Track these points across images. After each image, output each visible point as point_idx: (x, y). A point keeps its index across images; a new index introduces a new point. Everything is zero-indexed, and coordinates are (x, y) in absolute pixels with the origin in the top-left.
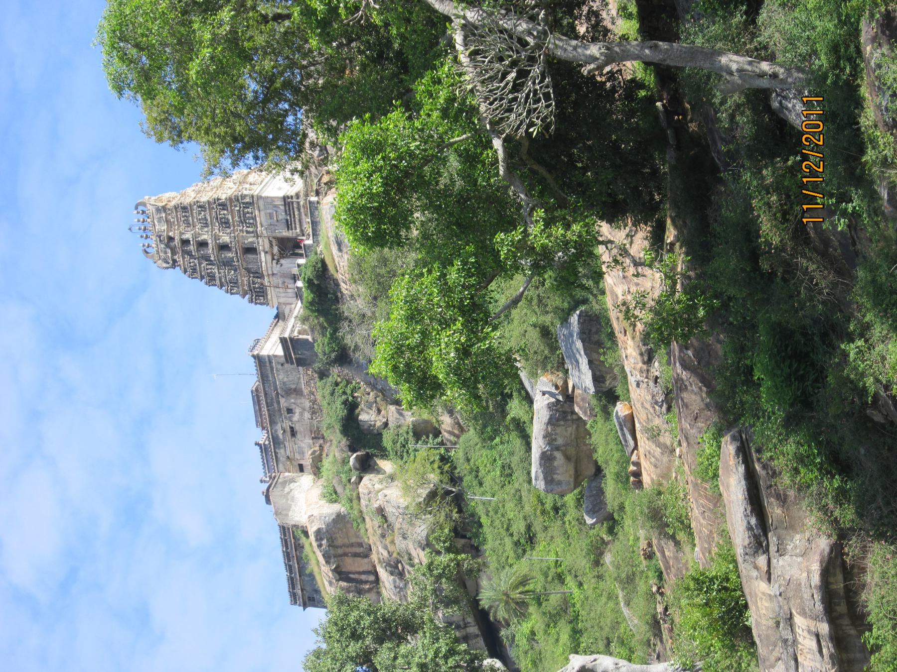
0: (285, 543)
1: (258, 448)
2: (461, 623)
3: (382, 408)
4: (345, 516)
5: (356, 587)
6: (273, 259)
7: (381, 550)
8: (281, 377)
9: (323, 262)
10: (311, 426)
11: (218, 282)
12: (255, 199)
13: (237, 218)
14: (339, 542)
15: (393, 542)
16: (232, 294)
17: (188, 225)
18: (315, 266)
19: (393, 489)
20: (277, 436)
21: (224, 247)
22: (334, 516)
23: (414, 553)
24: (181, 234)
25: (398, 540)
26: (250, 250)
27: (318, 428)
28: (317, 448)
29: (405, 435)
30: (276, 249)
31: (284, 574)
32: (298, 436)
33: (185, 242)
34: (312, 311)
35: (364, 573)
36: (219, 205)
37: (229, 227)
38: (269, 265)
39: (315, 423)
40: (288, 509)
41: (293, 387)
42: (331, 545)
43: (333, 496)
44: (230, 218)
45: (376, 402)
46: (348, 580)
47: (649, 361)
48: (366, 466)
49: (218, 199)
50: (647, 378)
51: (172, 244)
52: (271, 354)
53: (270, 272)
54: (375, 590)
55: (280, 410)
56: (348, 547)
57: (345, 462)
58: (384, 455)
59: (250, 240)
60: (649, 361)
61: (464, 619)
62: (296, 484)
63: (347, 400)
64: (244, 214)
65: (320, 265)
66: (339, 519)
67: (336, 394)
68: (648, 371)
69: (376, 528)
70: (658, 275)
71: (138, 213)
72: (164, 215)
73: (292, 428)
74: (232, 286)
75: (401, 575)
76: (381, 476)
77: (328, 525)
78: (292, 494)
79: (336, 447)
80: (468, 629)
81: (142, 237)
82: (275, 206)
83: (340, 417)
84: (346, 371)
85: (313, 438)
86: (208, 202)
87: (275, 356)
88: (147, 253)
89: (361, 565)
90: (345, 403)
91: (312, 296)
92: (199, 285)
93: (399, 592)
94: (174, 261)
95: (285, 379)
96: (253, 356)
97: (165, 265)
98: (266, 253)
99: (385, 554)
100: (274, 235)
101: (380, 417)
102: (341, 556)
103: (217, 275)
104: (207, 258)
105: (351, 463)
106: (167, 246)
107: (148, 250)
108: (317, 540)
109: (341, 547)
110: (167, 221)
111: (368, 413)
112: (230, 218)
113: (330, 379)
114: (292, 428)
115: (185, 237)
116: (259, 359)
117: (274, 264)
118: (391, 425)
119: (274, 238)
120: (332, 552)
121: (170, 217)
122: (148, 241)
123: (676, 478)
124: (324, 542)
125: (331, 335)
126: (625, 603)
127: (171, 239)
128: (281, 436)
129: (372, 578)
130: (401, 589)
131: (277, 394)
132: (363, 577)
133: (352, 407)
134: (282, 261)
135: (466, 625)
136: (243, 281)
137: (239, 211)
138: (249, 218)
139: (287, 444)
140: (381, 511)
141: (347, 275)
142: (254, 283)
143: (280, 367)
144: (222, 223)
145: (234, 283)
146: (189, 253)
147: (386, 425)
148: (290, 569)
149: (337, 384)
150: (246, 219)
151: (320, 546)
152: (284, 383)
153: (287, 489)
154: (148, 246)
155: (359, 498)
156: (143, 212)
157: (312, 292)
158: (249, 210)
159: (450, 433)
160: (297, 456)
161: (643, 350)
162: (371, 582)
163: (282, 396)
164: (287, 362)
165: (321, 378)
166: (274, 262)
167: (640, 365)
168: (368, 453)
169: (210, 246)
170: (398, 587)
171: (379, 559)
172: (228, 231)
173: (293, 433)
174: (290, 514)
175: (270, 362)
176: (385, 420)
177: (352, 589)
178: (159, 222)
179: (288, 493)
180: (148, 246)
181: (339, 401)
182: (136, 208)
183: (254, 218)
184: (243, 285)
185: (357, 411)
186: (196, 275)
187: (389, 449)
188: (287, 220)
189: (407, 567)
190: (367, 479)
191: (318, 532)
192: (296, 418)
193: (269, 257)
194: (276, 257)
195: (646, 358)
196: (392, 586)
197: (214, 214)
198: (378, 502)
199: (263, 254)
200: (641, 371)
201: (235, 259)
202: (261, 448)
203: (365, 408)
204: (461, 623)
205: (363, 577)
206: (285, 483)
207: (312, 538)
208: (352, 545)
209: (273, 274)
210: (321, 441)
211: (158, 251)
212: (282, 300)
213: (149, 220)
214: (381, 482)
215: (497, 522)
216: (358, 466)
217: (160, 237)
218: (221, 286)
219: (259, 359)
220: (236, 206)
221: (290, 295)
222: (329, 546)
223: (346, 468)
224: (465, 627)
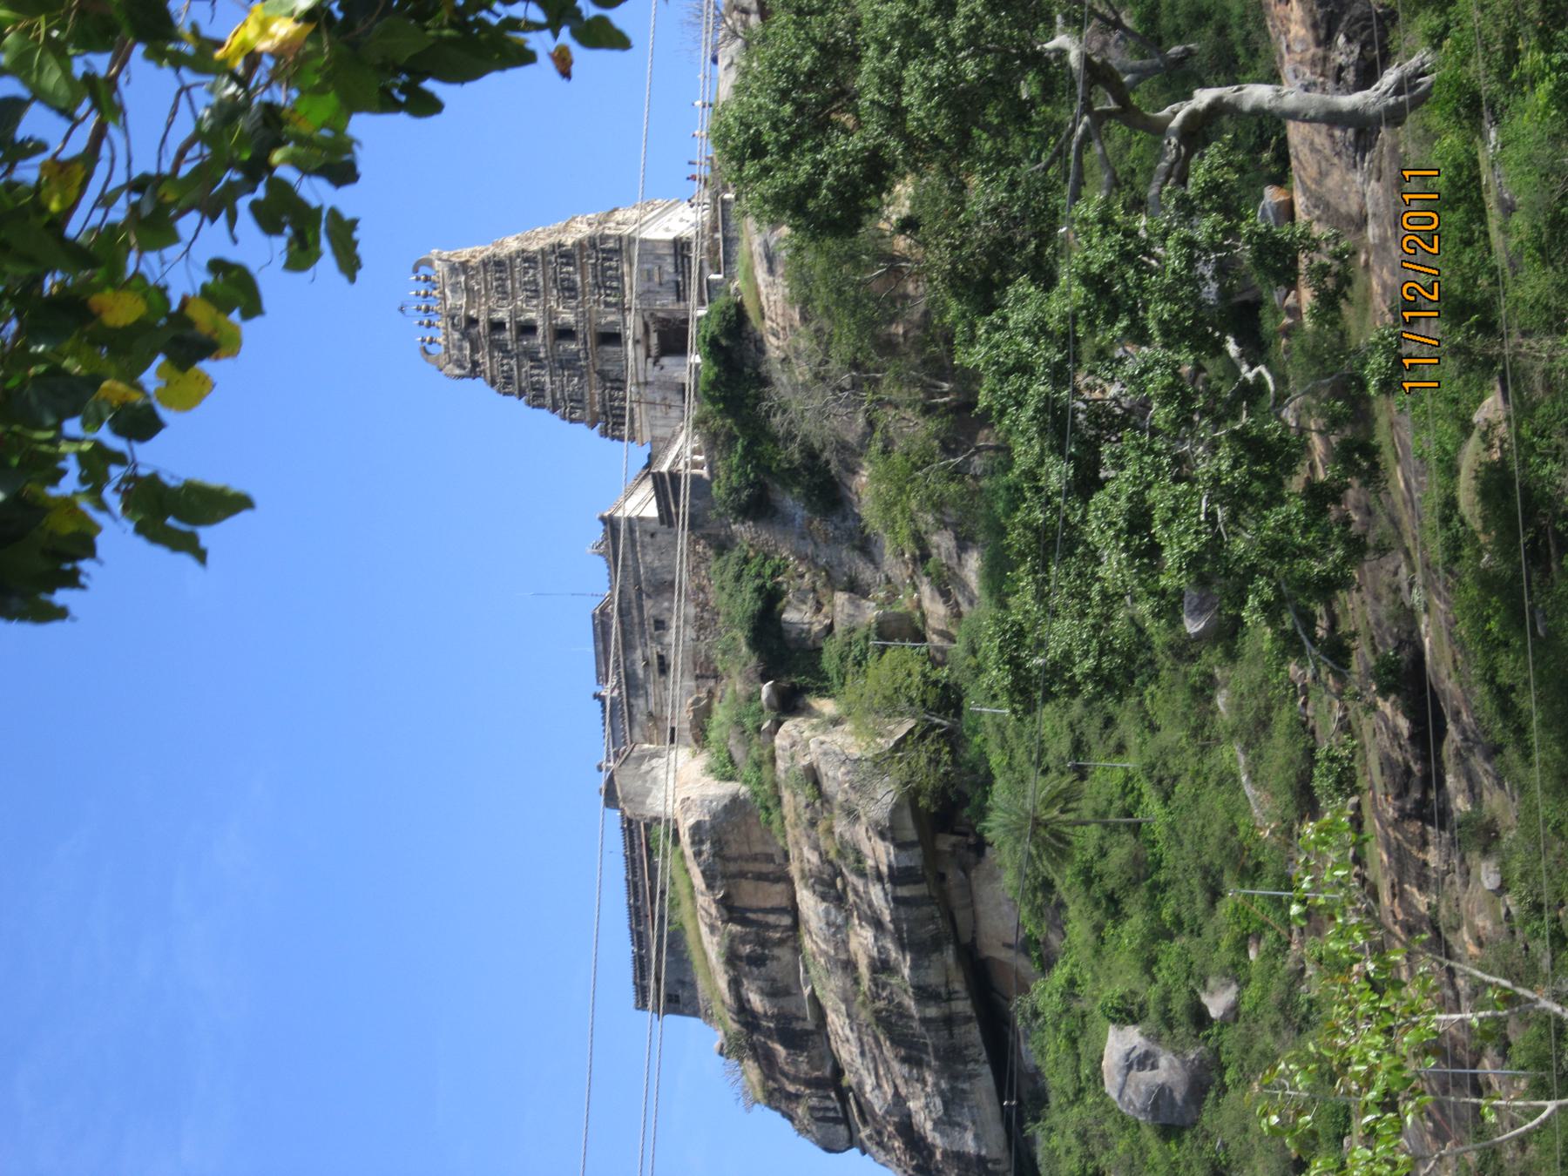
0: (631, 845)
1: (598, 703)
2: (943, 990)
3: (824, 601)
4: (745, 801)
5: (757, 934)
6: (648, 356)
8: (649, 559)
9: (740, 307)
10: (696, 653)
11: (548, 401)
13: (590, 280)
14: (732, 850)
15: (830, 831)
16: (572, 421)
17: (504, 294)
18: (724, 313)
19: (832, 741)
20: (635, 672)
21: (565, 333)
22: (726, 801)
23: (866, 848)
25: (841, 826)
26: (611, 338)
27: (707, 657)
28: (703, 695)
29: (862, 642)
30: (654, 339)
33: (497, 326)
34: (714, 401)
35: (773, 910)
36: (562, 256)
37: (575, 297)
38: (641, 365)
39: (703, 647)
42: (718, 853)
43: (726, 770)
44: (578, 278)
45: (814, 590)
46: (744, 922)
47: (1326, 41)
48: (789, 704)
49: (560, 245)
50: (1322, 75)
51: (473, 331)
52: (634, 515)
54: (790, 944)
55: (642, 623)
57: (752, 698)
58: (823, 692)
59: (611, 318)
60: (1326, 41)
61: (947, 984)
63: (763, 586)
64: (604, 270)
65: (733, 311)
66: (735, 806)
67: (745, 577)
68: (1325, 59)
69: (801, 810)
71: (418, 279)
72: (462, 278)
73: (661, 658)
74: (570, 407)
75: (840, 900)
76: (815, 721)
77: (714, 816)
78: (653, 773)
79: (741, 682)
80: (953, 1004)
81: (421, 324)
82: (659, 257)
83: (749, 613)
84: (765, 536)
85: (697, 677)
86: (542, 250)
87: (641, 519)
88: (425, 351)
89: (774, 895)
90: (760, 589)
91: (716, 369)
93: (834, 934)
94: (475, 364)
95: (657, 563)
96: (602, 519)
97: (458, 372)
99: (814, 858)
101: (821, 617)
102: (733, 876)
103: (548, 386)
104: (532, 355)
105: (764, 696)
106: (465, 335)
107: (431, 348)
108: (693, 843)
109: (735, 860)
110: (469, 290)
111: (800, 610)
112: (578, 278)
113: (736, 553)
114: (661, 658)
116: (610, 523)
117: (650, 365)
118: (838, 628)
120: (719, 867)
121: (473, 283)
122: (432, 331)
123: (1367, 262)
124: (706, 847)
125: (744, 448)
126: (1250, 776)
127: (472, 322)
128: (640, 673)
129: (786, 921)
130: (838, 928)
131: (640, 592)
132: (772, 919)
133: (771, 599)
134: (665, 361)
136: (592, 395)
137: (595, 265)
138: (611, 278)
139: (651, 689)
140: (812, 776)
141: (780, 320)
142: (612, 399)
143: (647, 539)
144: (564, 289)
145: (577, 400)
146: (501, 347)
147: (830, 629)
149: (746, 561)
150: (608, 282)
151: (698, 854)
152: (653, 570)
153: (645, 767)
154: (432, 341)
155: (773, 760)
156: (427, 279)
157: (716, 363)
158: (614, 264)
161: (1318, 17)
163: (649, 596)
165: (719, 554)
166: (650, 360)
167: (1313, 50)
168: (793, 684)
169: (540, 331)
170: (834, 924)
171: (802, 871)
172: (574, 303)
174: (649, 801)
175: (631, 531)
176: (828, 621)
177: (751, 937)
178: (453, 291)
179: (648, 772)
180: (432, 341)
181: (749, 587)
182: (416, 270)
183: (620, 279)
184: (592, 404)
185: (779, 606)
186: (510, 388)
187: (832, 674)
188: (677, 283)
189: (853, 879)
190: (789, 726)
191: (697, 828)
192: (671, 637)
193: (641, 351)
195: (1322, 33)
196: (823, 924)
197: (550, 272)
198: (808, 758)
200: (1313, 63)
201: (582, 355)
202: (603, 704)
203: (794, 602)
205: (772, 919)
206: (641, 758)
207: (685, 839)
208: (755, 858)
209: (646, 383)
210: (711, 683)
211: (447, 348)
212: (659, 432)
213: (435, 293)
214: (814, 728)
215: (1020, 755)
216: (775, 702)
217: (453, 318)
218: (554, 409)
219: (610, 523)
220: (589, 257)
222: (714, 855)
223: (754, 707)
224: (949, 999)
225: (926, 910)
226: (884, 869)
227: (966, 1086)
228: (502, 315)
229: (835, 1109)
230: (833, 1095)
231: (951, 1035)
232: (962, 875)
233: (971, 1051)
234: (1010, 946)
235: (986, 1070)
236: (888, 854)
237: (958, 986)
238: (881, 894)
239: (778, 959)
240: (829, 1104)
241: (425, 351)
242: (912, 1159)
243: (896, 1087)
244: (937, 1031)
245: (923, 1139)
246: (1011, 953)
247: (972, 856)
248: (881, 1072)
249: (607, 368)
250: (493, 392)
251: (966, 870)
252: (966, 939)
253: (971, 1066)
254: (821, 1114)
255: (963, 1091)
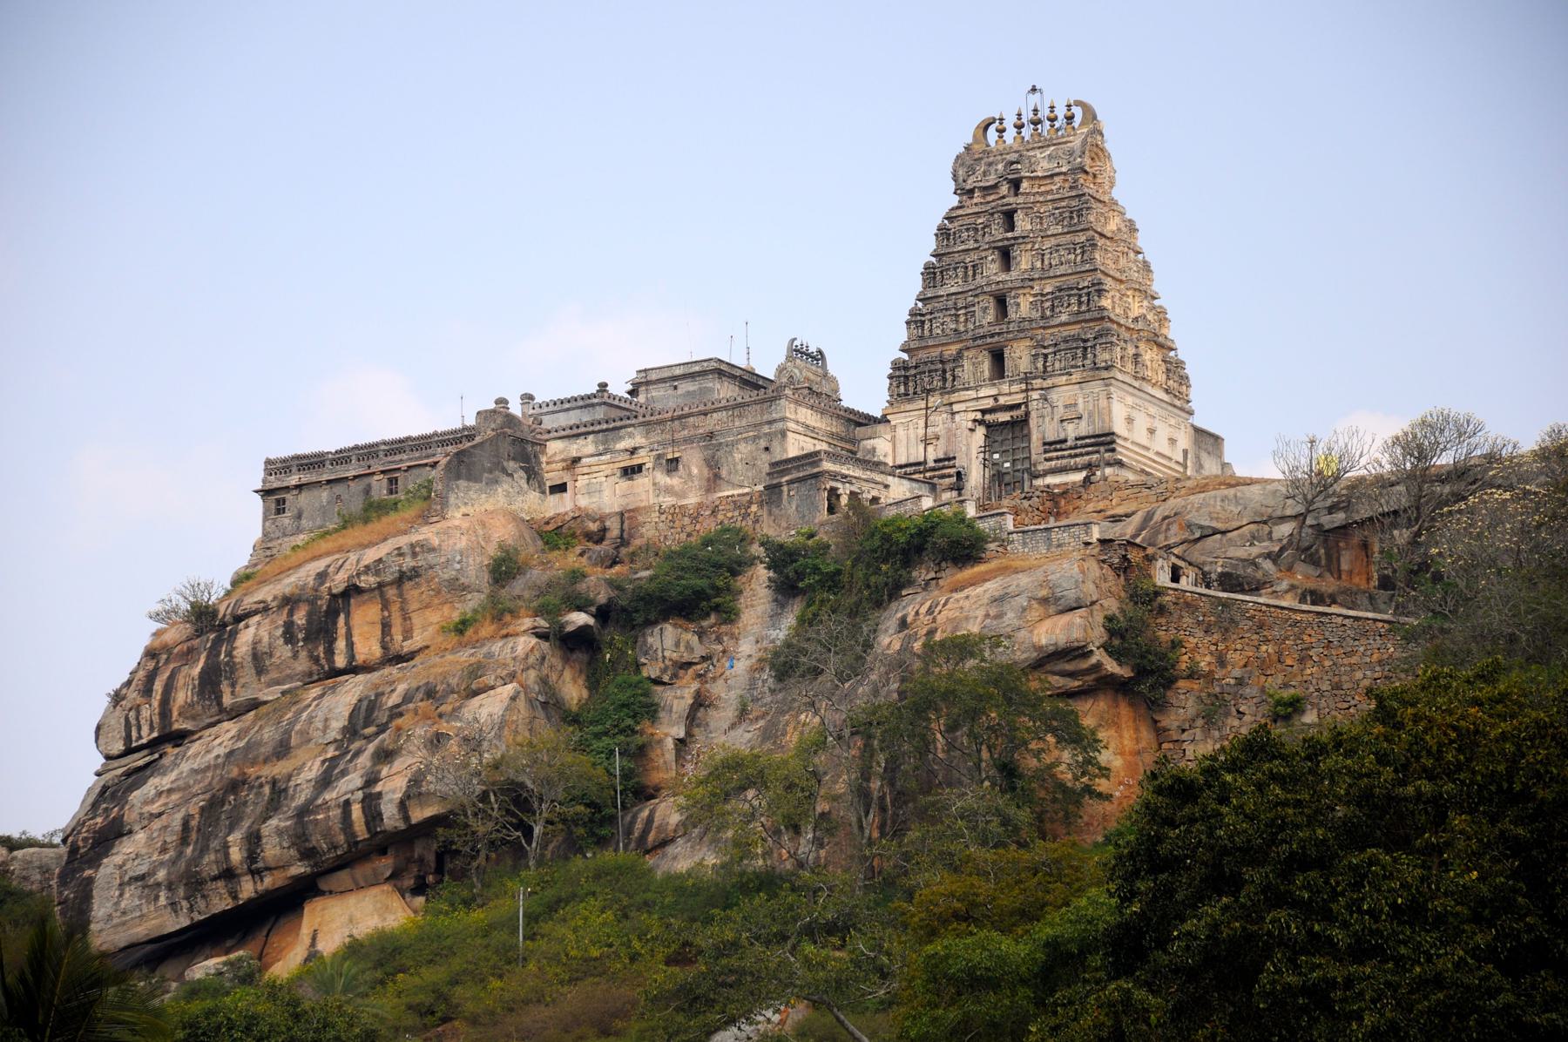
6: (984, 412)
7: (401, 688)
12: (1105, 374)
20: (621, 438)
23: (399, 764)
24: (1028, 209)
30: (1004, 417)
31: (330, 443)
32: (624, 484)
40: (472, 478)
41: (724, 473)
53: (956, 408)
56: (402, 609)
61: (268, 869)
62: (523, 483)
70: (1061, 396)
73: (637, 469)
88: (986, 127)
92: (924, 248)
95: (737, 456)
98: (995, 398)
100: (1033, 415)
107: (992, 129)
109: (401, 595)
112: (1064, 318)
115: (1019, 217)
117: (972, 416)
119: (1027, 414)
128: (621, 445)
134: (981, 431)
135: (256, 873)
143: (763, 443)
148: (342, 457)
153: (511, 465)
159: (650, 820)
160: (582, 481)
162: (330, 660)
164: (773, 465)
166: (979, 416)
173: (630, 472)
174: (462, 483)
179: (504, 471)
192: (662, 479)
193: (990, 403)
194: (988, 417)
199: (994, 391)
204: (260, 865)
205: (341, 644)
208: (406, 617)
221: (913, 451)
225: (341, 838)
226: (378, 788)
227: (163, 901)
228: (1023, 224)
229: (140, 737)
230: (155, 734)
231: (215, 879)
232: (388, 874)
233: (201, 904)
234: (314, 939)
235: (184, 922)
236: (394, 791)
237: (268, 882)
238: (351, 787)
239: (295, 656)
240: (145, 730)
241: (986, 127)
242: (85, 840)
243: (160, 814)
244: (217, 862)
245: (106, 852)
246: (307, 941)
247: (409, 882)
248: (175, 797)
249: (965, 363)
250: (938, 220)
251: (395, 876)
252: (323, 886)
253: (185, 904)
254: (133, 722)
255: (157, 898)
